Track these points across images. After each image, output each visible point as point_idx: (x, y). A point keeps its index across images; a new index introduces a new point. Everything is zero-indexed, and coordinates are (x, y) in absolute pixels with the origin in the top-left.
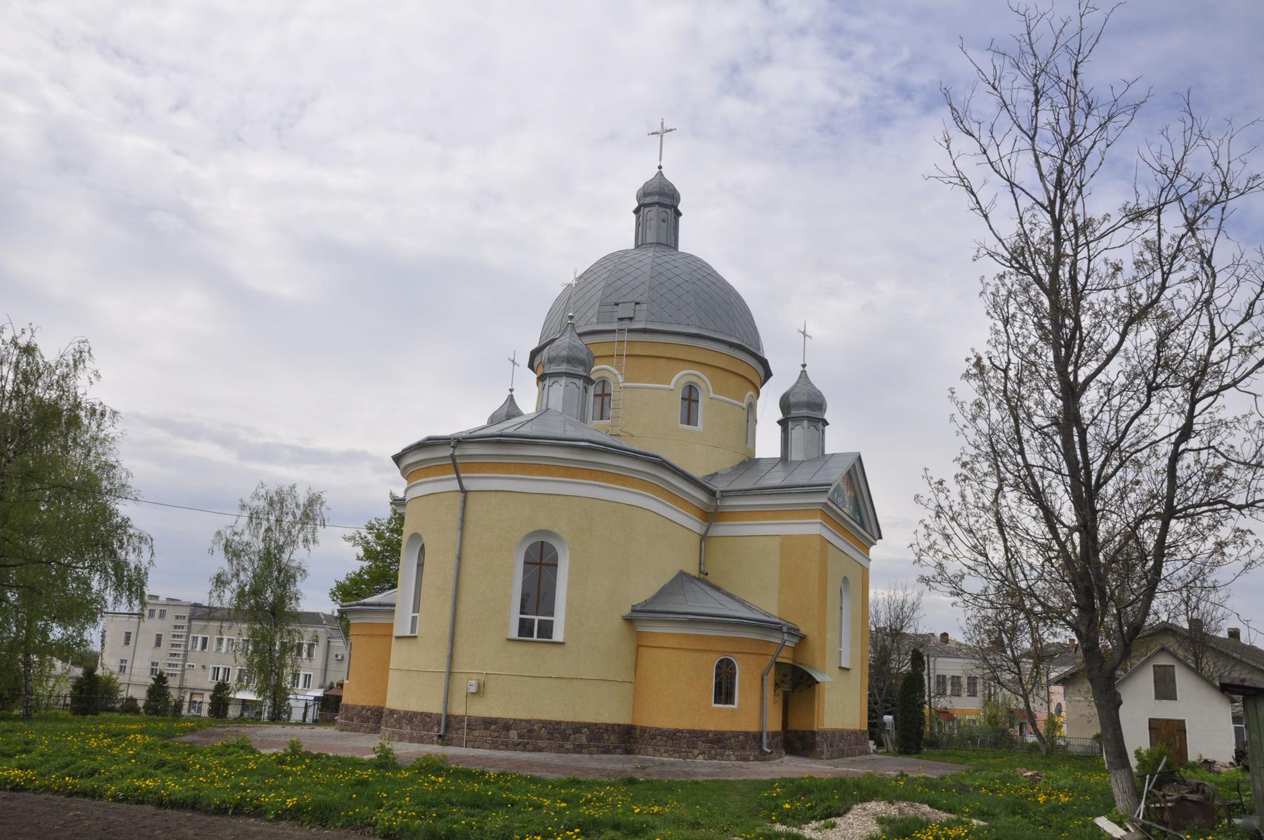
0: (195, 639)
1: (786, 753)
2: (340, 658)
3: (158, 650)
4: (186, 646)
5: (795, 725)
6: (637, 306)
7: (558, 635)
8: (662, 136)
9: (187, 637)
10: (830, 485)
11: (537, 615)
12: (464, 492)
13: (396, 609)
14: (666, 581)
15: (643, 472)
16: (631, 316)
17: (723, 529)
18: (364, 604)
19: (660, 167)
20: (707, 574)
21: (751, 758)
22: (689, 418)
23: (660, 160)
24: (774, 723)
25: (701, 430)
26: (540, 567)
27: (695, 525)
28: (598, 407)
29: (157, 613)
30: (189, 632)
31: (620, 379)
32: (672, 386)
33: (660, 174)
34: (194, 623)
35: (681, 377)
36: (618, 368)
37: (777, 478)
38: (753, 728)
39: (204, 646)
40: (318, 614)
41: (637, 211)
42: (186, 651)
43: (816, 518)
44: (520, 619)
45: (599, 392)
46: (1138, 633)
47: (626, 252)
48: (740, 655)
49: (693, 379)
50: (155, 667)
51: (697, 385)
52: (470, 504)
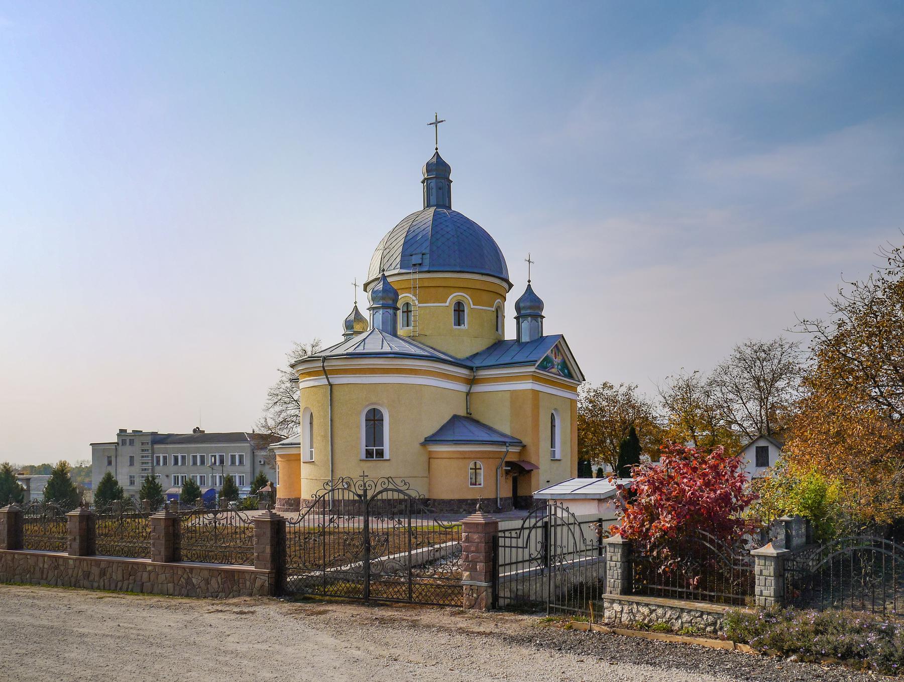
0: (158, 458)
1: (515, 508)
2: (262, 463)
3: (132, 468)
4: (152, 463)
5: (521, 492)
6: (424, 256)
7: (387, 456)
8: (436, 126)
9: (152, 457)
10: (536, 361)
11: (375, 447)
12: (331, 385)
13: (301, 446)
14: (445, 421)
15: (440, 352)
16: (421, 262)
17: (478, 388)
18: (283, 444)
20: (471, 414)
21: (492, 511)
22: (459, 321)
24: (506, 491)
25: (467, 328)
26: (374, 418)
27: (463, 388)
28: (405, 319)
29: (128, 441)
30: (153, 453)
31: (417, 302)
32: (447, 304)
34: (156, 446)
35: (453, 298)
36: (415, 295)
38: (492, 496)
39: (165, 463)
40: (243, 433)
42: (153, 466)
43: (530, 380)
44: (366, 449)
45: (405, 310)
48: (483, 460)
49: (460, 298)
50: (132, 479)
52: (334, 391)
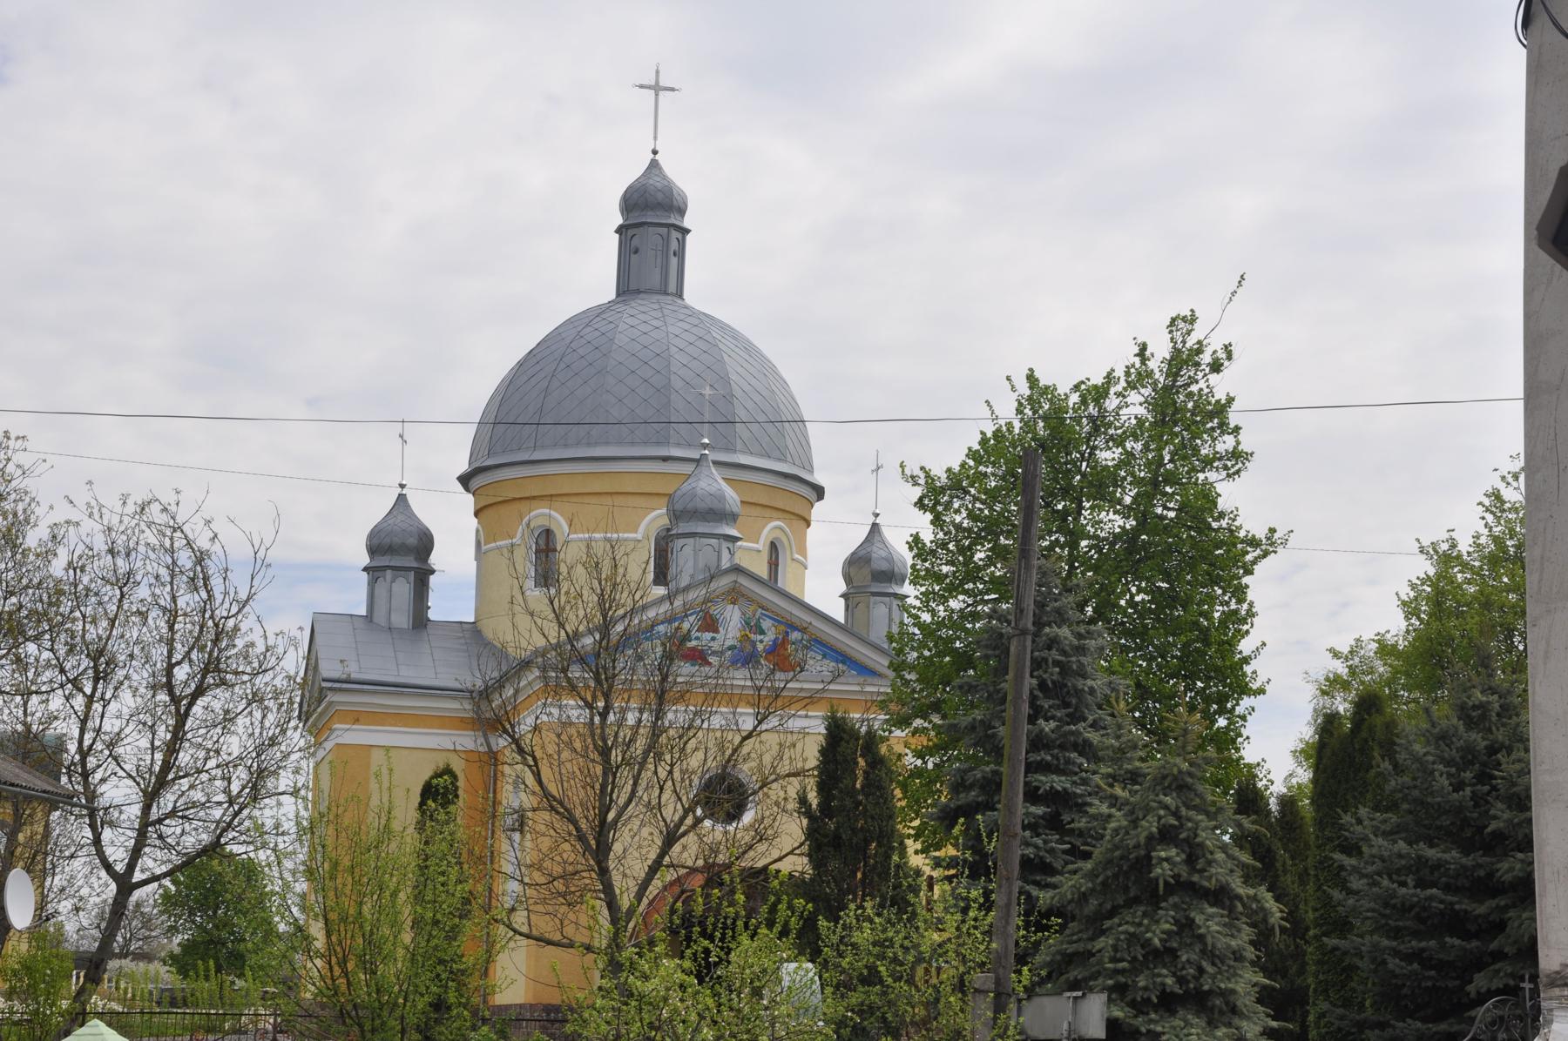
19: (655, 152)
23: (655, 138)
33: (654, 165)
37: (1397, 836)
41: (619, 230)
46: (128, 864)
47: (601, 311)
51: (782, 542)
